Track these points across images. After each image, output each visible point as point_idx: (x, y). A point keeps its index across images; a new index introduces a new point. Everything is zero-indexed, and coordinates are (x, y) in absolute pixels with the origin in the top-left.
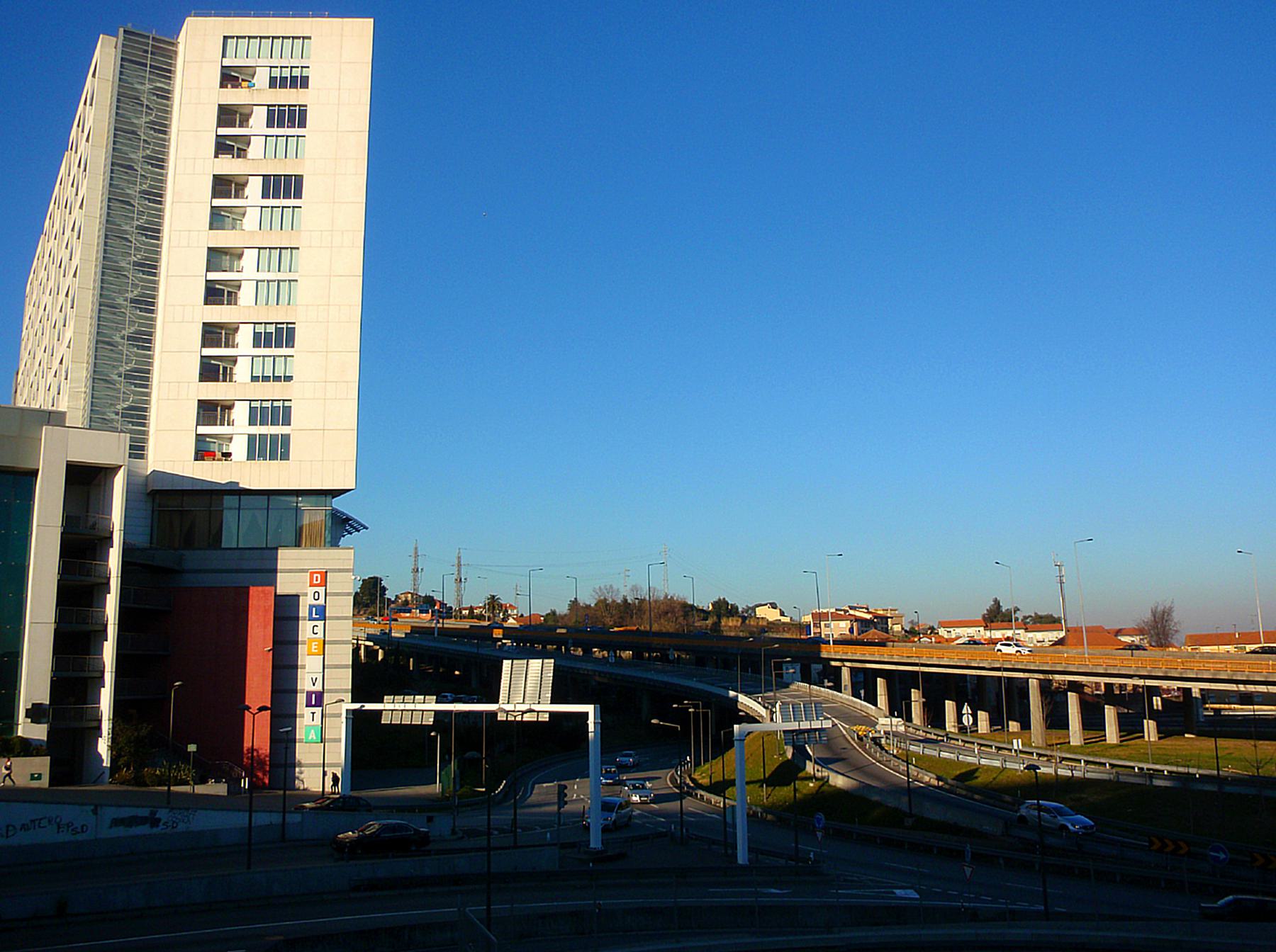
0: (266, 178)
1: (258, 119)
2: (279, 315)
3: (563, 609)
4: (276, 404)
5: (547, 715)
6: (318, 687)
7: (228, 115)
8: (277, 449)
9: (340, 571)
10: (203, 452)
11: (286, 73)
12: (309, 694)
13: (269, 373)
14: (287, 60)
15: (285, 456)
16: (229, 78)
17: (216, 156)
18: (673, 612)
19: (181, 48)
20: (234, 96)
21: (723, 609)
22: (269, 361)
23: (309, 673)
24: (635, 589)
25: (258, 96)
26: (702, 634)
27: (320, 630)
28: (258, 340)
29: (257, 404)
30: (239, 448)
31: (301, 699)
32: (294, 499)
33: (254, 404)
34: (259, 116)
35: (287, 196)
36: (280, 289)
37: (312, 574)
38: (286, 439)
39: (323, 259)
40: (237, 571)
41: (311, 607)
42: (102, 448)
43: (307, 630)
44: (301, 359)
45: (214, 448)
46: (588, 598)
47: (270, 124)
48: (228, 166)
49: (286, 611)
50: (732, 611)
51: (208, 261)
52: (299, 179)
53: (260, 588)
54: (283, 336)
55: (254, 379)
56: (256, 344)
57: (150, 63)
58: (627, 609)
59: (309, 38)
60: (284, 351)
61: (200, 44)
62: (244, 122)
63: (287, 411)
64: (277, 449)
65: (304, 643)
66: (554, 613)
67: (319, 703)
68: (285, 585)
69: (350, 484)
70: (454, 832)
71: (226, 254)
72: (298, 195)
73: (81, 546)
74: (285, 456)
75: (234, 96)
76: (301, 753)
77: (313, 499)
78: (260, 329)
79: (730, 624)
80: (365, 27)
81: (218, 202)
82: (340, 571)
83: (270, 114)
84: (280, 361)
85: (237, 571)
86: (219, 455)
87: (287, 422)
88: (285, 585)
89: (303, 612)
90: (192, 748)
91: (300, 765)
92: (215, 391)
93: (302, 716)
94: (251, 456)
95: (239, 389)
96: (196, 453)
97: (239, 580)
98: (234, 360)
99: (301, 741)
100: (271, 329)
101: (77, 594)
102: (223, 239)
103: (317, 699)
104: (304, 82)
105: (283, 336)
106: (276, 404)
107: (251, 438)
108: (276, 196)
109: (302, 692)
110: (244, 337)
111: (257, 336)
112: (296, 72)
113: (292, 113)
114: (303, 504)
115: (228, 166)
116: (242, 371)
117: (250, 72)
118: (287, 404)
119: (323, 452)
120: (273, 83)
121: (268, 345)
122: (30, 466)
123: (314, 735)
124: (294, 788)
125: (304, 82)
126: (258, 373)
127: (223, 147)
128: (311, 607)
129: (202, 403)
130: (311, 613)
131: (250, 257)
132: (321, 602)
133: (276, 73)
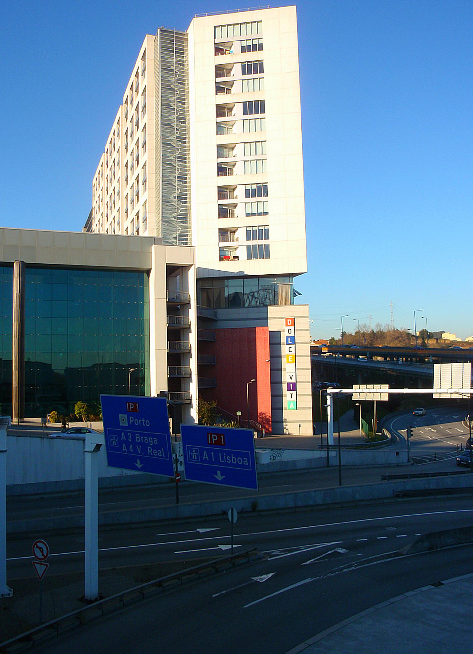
0: (244, 103)
1: (237, 71)
2: (258, 179)
3: (338, 337)
4: (260, 228)
5: (469, 395)
6: (293, 381)
7: (220, 70)
8: (263, 253)
9: (301, 317)
10: (223, 257)
11: (250, 43)
12: (289, 384)
13: (255, 211)
14: (248, 35)
15: (268, 256)
16: (219, 50)
17: (216, 94)
18: (402, 337)
19: (189, 37)
20: (222, 60)
21: (425, 335)
22: (255, 205)
23: (288, 372)
24: (378, 325)
25: (235, 57)
26: (416, 348)
27: (292, 349)
28: (248, 194)
29: (250, 229)
30: (242, 252)
31: (285, 387)
32: (273, 279)
33: (248, 229)
34: (237, 69)
35: (257, 112)
36: (259, 162)
37: (287, 319)
38: (267, 246)
39: (280, 145)
40: (247, 319)
41: (287, 337)
42: (175, 255)
43: (285, 349)
44: (271, 202)
45: (228, 254)
46: (351, 330)
47: (244, 73)
48: (223, 99)
49: (274, 339)
50: (430, 336)
51: (218, 152)
52: (263, 102)
53: (261, 328)
54: (261, 190)
55: (248, 215)
56: (247, 196)
57: (174, 46)
58: (374, 335)
59: (261, 21)
60: (262, 199)
61: (201, 33)
62: (229, 72)
63: (267, 231)
64: (263, 253)
65: (284, 356)
66: (333, 339)
67: (294, 389)
68: (273, 326)
69: (302, 268)
70: (409, 461)
71: (226, 148)
72: (263, 111)
73: (176, 308)
74: (268, 256)
75: (222, 60)
76: (286, 415)
77: (281, 279)
78: (248, 187)
79: (431, 343)
80: (294, 8)
81: (220, 119)
82: (301, 317)
83: (243, 67)
84: (261, 205)
85: (247, 319)
86: (231, 258)
87: (267, 238)
88: (273, 326)
89: (283, 340)
90: (239, 413)
91: (286, 421)
92: (226, 223)
93: (286, 396)
94: (249, 257)
95: (239, 221)
96: (220, 257)
97: (249, 324)
98: (235, 206)
99: (286, 409)
100: (254, 187)
101: (176, 334)
102: (224, 139)
103: (293, 387)
104: (260, 47)
105: (261, 190)
106: (260, 228)
107: (248, 247)
108: (251, 113)
109: (285, 383)
110: (240, 192)
111: (247, 191)
112: (255, 42)
113: (255, 65)
114: (277, 281)
115: (223, 99)
116: (239, 211)
117: (230, 45)
118: (266, 228)
119: (287, 254)
120: (243, 49)
121: (253, 196)
122: (147, 267)
123: (293, 406)
124: (283, 434)
125: (260, 47)
126: (249, 211)
127: (219, 89)
128: (287, 337)
129: (218, 146)
130: (287, 341)
131: (238, 150)
132: (292, 334)
133: (244, 44)
